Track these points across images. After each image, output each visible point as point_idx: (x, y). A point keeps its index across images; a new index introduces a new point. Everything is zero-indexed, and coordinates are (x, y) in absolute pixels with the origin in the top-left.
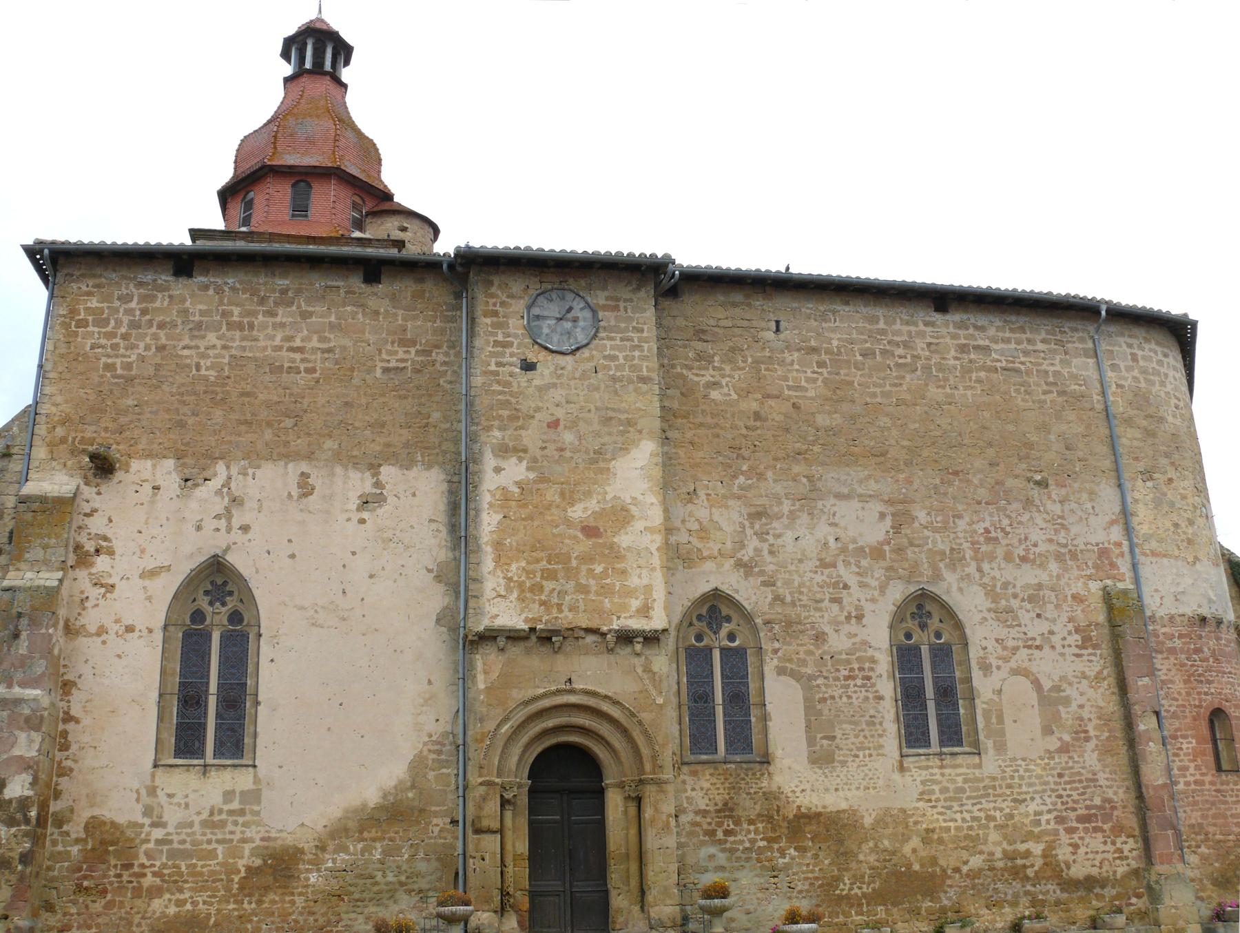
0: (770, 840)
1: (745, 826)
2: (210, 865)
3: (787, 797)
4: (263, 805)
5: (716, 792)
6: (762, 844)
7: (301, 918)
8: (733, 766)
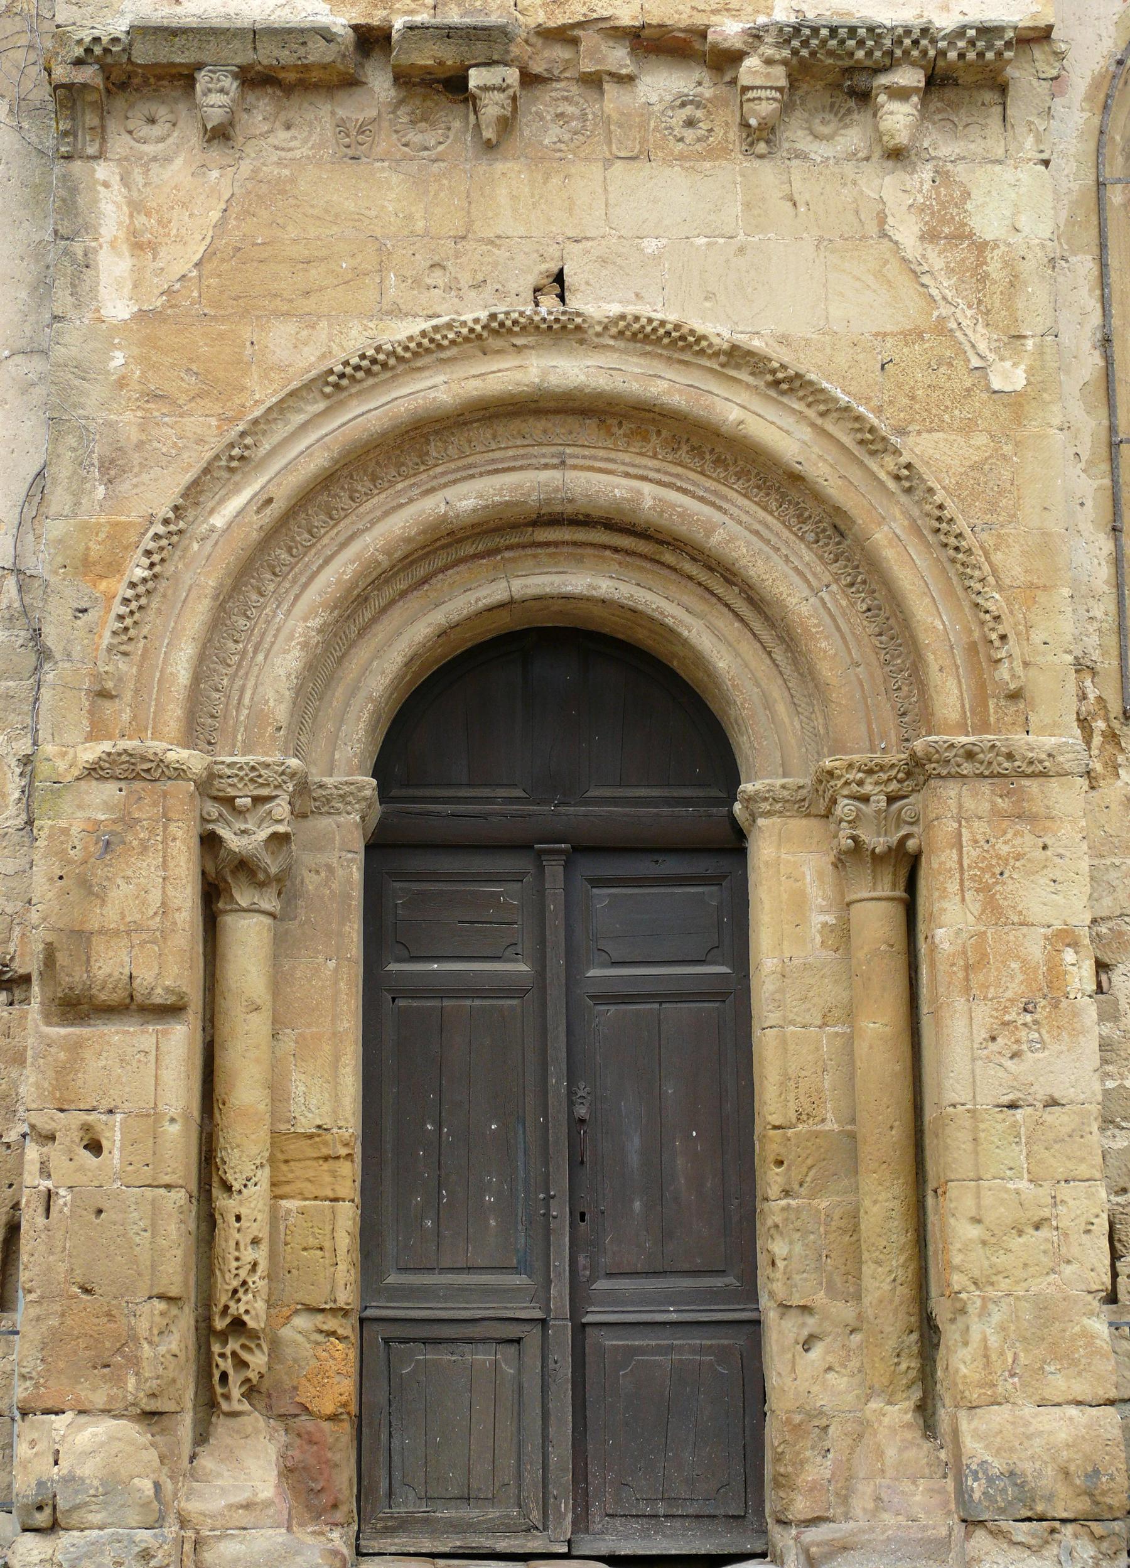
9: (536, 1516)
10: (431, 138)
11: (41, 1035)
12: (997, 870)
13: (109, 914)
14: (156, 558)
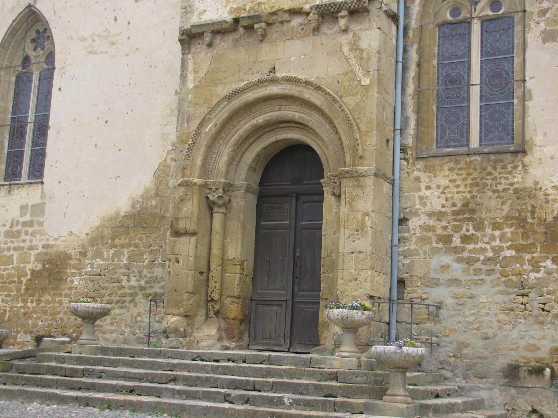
0: (520, 249)
1: (489, 231)
2: (8, 269)
3: (546, 195)
4: (45, 217)
5: (455, 190)
6: (509, 253)
7: (65, 317)
8: (478, 158)
9: (282, 343)
10: (252, 39)
11: (169, 239)
12: (353, 199)
13: (182, 215)
14: (194, 139)
